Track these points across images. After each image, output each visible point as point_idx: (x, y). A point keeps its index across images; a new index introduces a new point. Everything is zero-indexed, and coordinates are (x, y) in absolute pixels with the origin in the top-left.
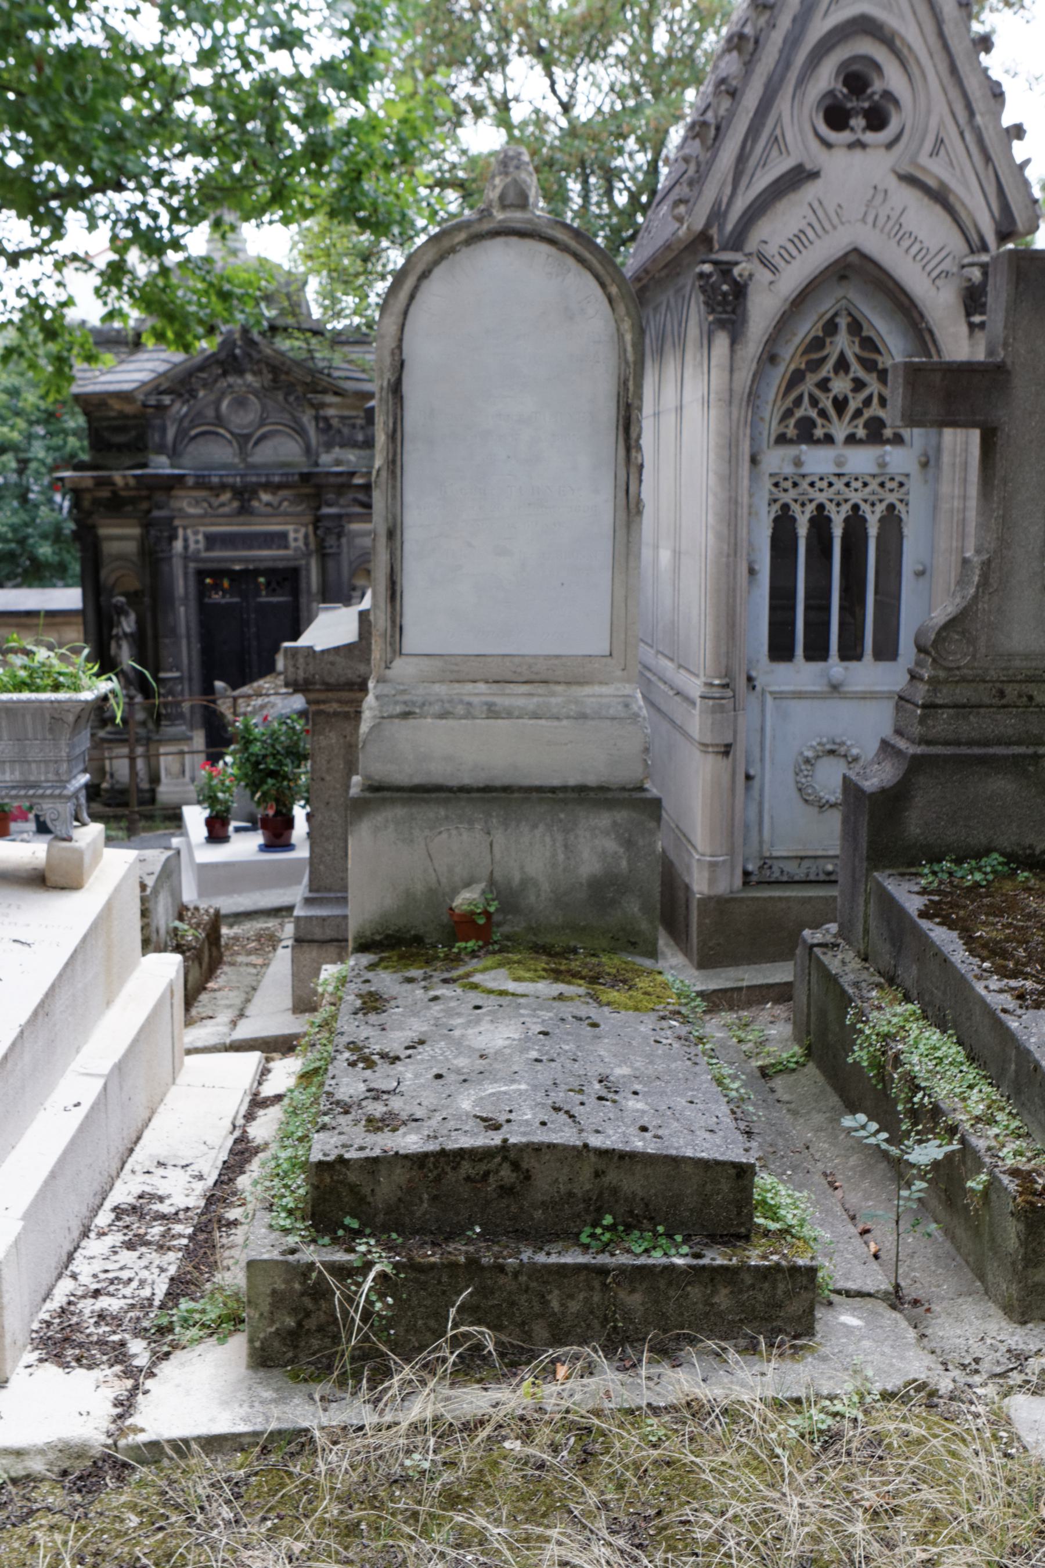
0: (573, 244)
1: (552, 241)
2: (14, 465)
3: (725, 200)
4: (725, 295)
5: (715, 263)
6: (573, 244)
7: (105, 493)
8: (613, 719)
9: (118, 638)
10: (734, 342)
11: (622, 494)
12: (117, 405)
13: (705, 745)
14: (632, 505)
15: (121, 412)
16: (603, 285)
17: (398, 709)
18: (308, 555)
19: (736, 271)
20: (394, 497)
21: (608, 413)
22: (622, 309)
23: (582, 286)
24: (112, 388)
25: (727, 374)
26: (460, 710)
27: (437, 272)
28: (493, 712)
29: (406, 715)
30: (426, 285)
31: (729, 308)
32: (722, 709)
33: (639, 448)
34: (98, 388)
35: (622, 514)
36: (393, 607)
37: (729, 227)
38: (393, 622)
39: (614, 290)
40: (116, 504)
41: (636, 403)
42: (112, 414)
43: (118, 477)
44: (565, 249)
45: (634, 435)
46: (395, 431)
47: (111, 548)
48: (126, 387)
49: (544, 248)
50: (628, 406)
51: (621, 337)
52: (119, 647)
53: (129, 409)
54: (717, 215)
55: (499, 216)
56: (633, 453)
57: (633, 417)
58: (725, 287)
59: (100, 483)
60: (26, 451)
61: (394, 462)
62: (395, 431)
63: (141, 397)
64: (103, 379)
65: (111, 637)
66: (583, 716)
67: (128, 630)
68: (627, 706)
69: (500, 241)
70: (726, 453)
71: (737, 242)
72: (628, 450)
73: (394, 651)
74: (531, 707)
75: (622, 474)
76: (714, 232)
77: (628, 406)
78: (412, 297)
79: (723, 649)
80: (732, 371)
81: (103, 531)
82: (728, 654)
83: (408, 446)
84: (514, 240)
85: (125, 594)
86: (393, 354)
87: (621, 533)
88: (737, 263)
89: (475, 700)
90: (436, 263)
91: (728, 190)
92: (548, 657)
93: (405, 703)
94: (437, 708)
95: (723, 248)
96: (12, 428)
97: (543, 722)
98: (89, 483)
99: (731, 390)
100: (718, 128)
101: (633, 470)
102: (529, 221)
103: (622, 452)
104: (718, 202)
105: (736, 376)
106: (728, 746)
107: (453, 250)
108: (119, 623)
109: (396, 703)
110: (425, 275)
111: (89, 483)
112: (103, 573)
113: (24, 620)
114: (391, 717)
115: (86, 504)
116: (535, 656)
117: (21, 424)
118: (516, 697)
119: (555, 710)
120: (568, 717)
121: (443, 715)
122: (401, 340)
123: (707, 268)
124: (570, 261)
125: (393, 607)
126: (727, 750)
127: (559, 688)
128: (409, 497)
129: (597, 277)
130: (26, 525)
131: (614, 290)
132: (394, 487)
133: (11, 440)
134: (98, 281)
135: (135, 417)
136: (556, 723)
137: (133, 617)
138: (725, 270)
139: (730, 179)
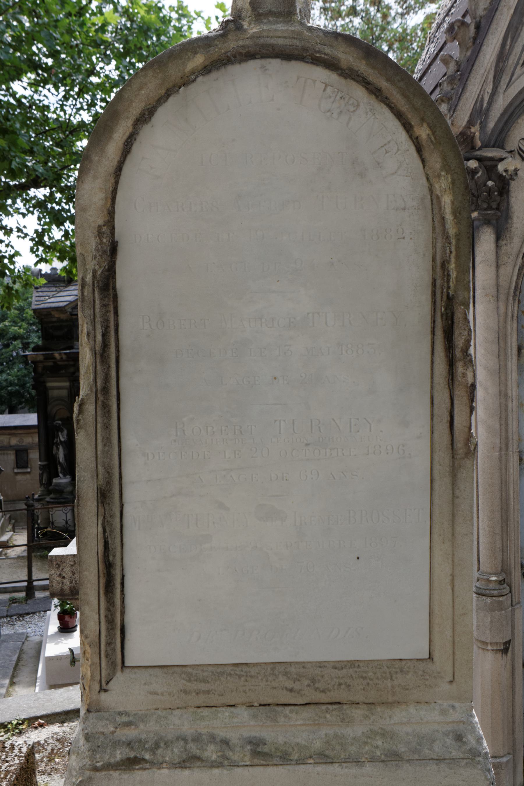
0: (362, 66)
1: (331, 65)
2: (20, 346)
3: (486, 98)
4: (490, 191)
5: (480, 159)
6: (362, 66)
7: (50, 363)
8: (440, 760)
9: (57, 444)
10: (498, 238)
11: (442, 428)
12: (57, 315)
13: (485, 643)
14: (459, 444)
15: (59, 318)
16: (408, 127)
17: (119, 755)
18: (442, 195)
19: (501, 167)
20: (107, 441)
21: (418, 310)
22: (435, 161)
23: (378, 129)
24: (53, 305)
25: (493, 268)
26: (211, 752)
27: (163, 113)
28: (261, 753)
29: (131, 764)
30: (146, 131)
31: (494, 205)
32: (500, 607)
33: (470, 362)
34: (46, 306)
35: (443, 456)
36: (110, 602)
37: (491, 125)
38: (110, 622)
39: (423, 132)
40: (56, 370)
41: (461, 295)
42: (54, 320)
43: (57, 355)
44: (349, 74)
45: (459, 342)
46: (105, 345)
47: (54, 394)
48: (61, 304)
49: (320, 73)
50: (450, 300)
51: (435, 200)
52: (58, 449)
53: (63, 316)
54: (480, 113)
55: (252, 29)
56: (460, 368)
57: (458, 316)
58: (490, 183)
59: (47, 358)
60: (27, 338)
61: (105, 390)
62: (105, 345)
63: (70, 310)
64: (49, 301)
65: (53, 444)
66: (393, 758)
67: (62, 440)
68: (459, 738)
69: (253, 65)
70: (495, 348)
71: (499, 139)
72: (451, 363)
73: (112, 665)
74: (318, 745)
75: (442, 396)
76: (475, 130)
77: (450, 300)
78: (127, 150)
79: (499, 545)
80: (498, 266)
81: (49, 384)
82: (503, 549)
83: (126, 366)
84: (275, 63)
85: (60, 419)
86: (100, 234)
87: (443, 485)
88: (502, 160)
89: (234, 736)
90: (162, 100)
91: (489, 89)
92: (339, 666)
93: (129, 744)
94: (175, 752)
95: (486, 145)
96: (20, 327)
97: (336, 768)
98: (41, 358)
99: (498, 285)
100: (478, 27)
101: (460, 394)
102: (297, 36)
103: (441, 367)
104: (480, 100)
105: (502, 271)
106: (507, 643)
107: (186, 81)
108: (58, 436)
109: (116, 744)
110: (145, 117)
111: (41, 358)
112: (49, 408)
113: (13, 431)
114: (108, 767)
115: (40, 369)
116: (321, 665)
117: (25, 325)
118: (293, 730)
119: (353, 749)
120: (373, 760)
121: (189, 761)
122: (111, 213)
123: (473, 164)
124: (359, 92)
125: (110, 602)
126: (506, 648)
127: (358, 713)
128: (131, 440)
129: (399, 115)
130: (25, 376)
131: (423, 132)
132: (107, 427)
133: (19, 333)
134: (31, 244)
135: (66, 321)
136: (354, 770)
137: (65, 432)
138: (490, 166)
139: (491, 77)
